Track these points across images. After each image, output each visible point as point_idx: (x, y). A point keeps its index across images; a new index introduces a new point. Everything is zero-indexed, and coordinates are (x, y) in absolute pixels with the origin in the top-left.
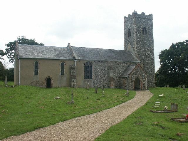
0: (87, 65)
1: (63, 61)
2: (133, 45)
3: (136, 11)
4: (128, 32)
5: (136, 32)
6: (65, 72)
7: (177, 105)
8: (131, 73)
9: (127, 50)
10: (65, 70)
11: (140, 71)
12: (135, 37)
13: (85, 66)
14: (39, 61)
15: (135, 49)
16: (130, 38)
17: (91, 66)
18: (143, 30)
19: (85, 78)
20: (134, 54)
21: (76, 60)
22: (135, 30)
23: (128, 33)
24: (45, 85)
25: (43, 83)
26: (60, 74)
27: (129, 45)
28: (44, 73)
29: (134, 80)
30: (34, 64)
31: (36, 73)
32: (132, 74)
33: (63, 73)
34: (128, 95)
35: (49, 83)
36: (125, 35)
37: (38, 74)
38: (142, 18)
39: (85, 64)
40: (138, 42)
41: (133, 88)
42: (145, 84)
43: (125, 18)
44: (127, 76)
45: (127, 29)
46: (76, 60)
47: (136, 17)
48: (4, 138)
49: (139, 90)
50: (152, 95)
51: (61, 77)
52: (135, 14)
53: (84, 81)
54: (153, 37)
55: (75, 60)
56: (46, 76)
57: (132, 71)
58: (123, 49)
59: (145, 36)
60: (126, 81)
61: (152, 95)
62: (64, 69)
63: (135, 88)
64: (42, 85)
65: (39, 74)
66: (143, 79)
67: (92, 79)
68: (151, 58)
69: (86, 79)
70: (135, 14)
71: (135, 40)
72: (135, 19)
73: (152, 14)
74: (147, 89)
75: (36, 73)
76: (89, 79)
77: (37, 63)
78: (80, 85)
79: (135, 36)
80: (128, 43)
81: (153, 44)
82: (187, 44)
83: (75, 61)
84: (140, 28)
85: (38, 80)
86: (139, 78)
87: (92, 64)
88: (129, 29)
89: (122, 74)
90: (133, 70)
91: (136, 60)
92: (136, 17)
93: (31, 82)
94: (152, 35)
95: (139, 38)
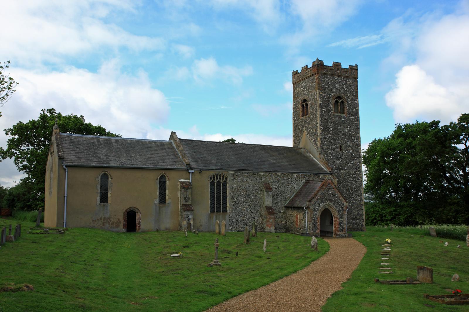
0: (216, 181)
1: (164, 171)
2: (312, 135)
3: (320, 59)
4: (303, 106)
5: (321, 107)
6: (167, 197)
7: (431, 271)
8: (313, 198)
9: (301, 146)
10: (167, 192)
11: (334, 194)
12: (319, 119)
13: (212, 184)
14: (110, 172)
15: (319, 145)
16: (306, 118)
17: (225, 185)
18: (337, 102)
19: (212, 211)
20: (317, 155)
21: (193, 171)
22: (319, 102)
23: (302, 108)
24: (122, 227)
25: (119, 222)
26: (157, 201)
27: (305, 136)
28: (294, 77)
29: (318, 213)
30: (100, 179)
31: (104, 199)
32: (314, 200)
33: (163, 199)
34: (315, 248)
35: (131, 221)
36: (294, 112)
37: (107, 202)
38: (333, 75)
39: (211, 178)
40: (325, 130)
41: (318, 232)
42: (344, 222)
43: (295, 73)
44: (304, 206)
45: (300, 100)
46: (193, 171)
47: (321, 73)
48: (88, 129)
49: (332, 236)
50: (364, 250)
51: (160, 207)
52: (319, 65)
53: (210, 217)
54: (358, 118)
55: (190, 171)
56: (127, 206)
57: (316, 195)
58: (292, 146)
59: (340, 117)
60: (300, 216)
61: (364, 250)
62: (165, 190)
63: (321, 231)
64: (118, 226)
65: (109, 202)
66: (339, 211)
67: (225, 211)
68: (353, 165)
69: (220, 211)
70: (319, 65)
71: (318, 125)
72: (318, 78)
73: (356, 66)
74: (350, 236)
75: (104, 199)
76: (219, 211)
77: (105, 177)
78: (201, 225)
79: (318, 115)
80: (302, 131)
81: (359, 133)
82: (468, 126)
83: (190, 173)
84: (329, 98)
85: (107, 216)
86: (331, 209)
87: (226, 178)
88: (305, 101)
89: (293, 201)
90: (318, 191)
91: (326, 171)
92: (321, 73)
93: (93, 221)
94: (357, 114)
95: (327, 120)
